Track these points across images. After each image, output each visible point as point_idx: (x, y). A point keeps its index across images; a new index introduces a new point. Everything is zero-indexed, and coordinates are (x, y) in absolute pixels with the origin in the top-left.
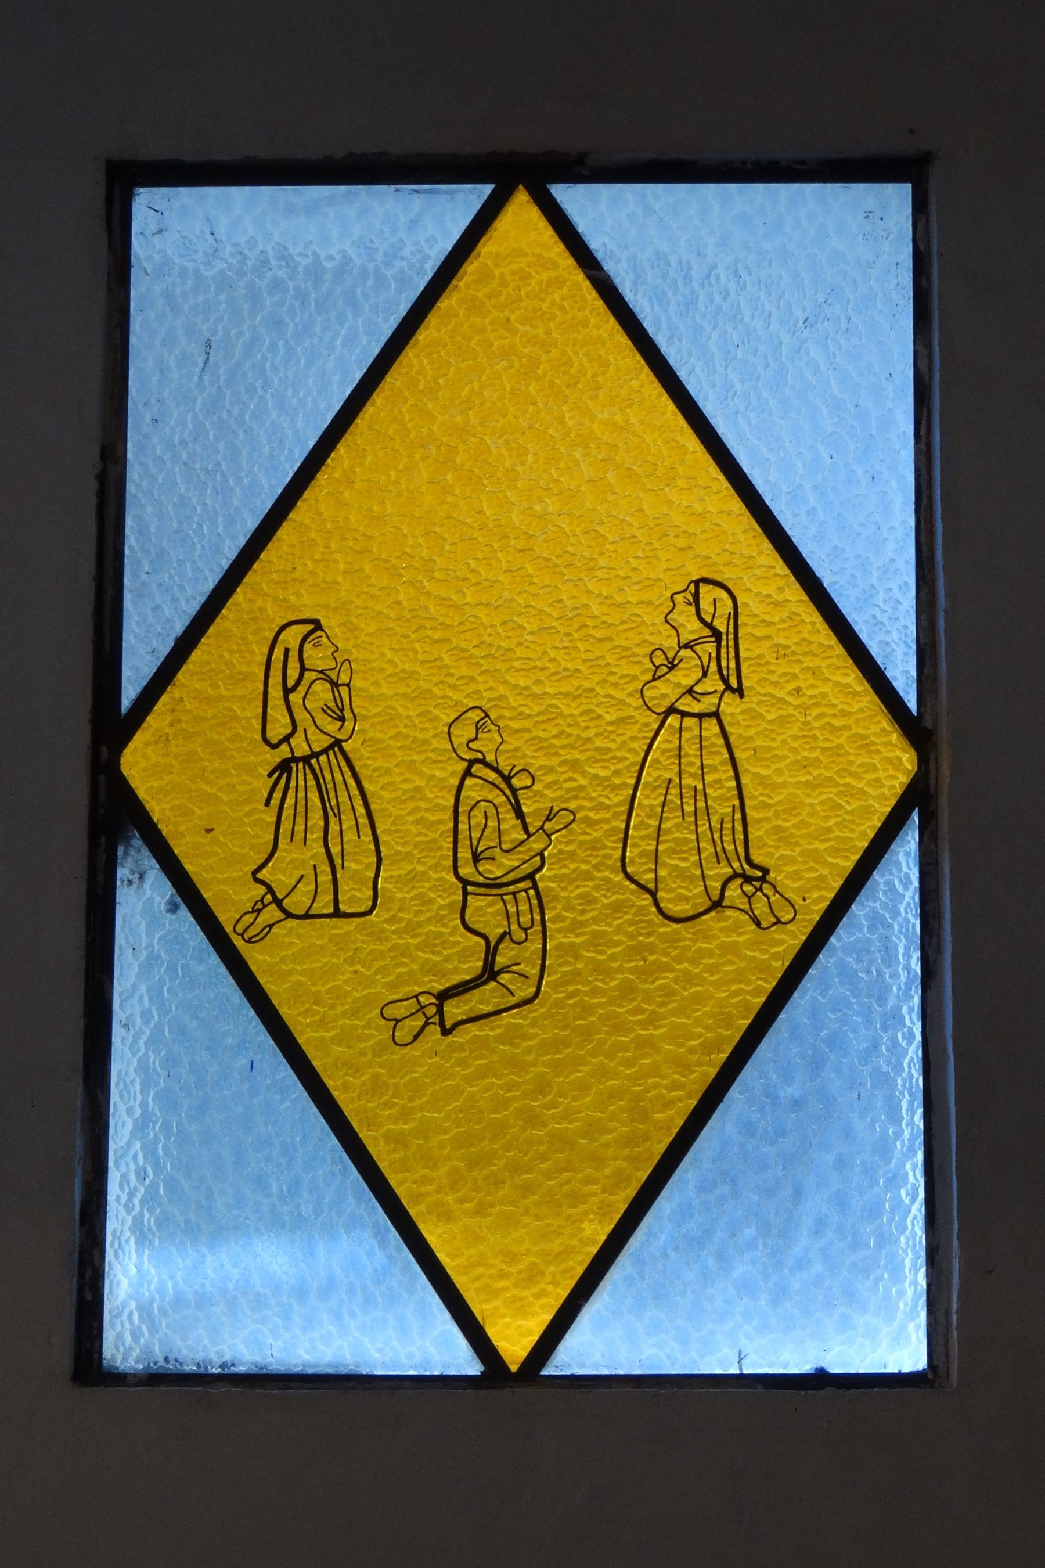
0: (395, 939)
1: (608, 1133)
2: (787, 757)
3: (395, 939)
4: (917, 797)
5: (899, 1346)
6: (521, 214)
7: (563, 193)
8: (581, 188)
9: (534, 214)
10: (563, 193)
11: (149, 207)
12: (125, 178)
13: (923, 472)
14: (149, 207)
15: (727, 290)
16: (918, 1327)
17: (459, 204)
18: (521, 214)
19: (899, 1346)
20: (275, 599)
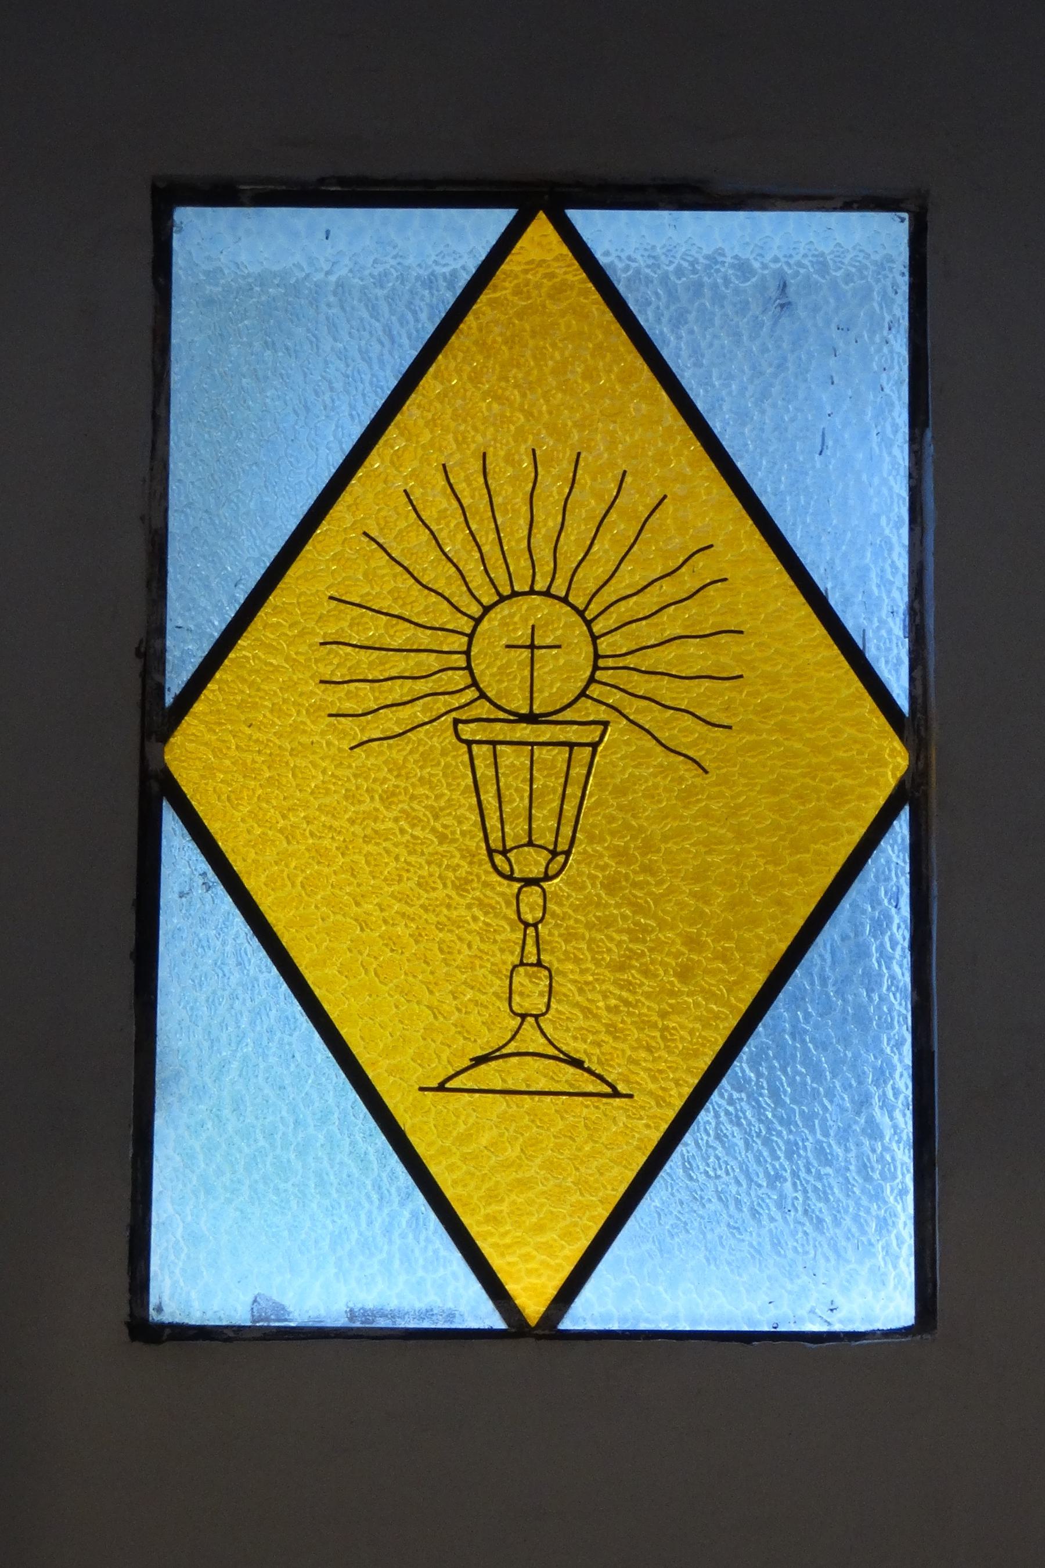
0: (877, 288)
1: (869, 338)
2: (692, 845)
3: (877, 288)
4: (907, 794)
5: (880, 1296)
6: (542, 229)
7: (576, 216)
8: (597, 213)
9: (549, 229)
10: (576, 216)
11: (184, 215)
12: (168, 196)
13: (918, 683)
14: (184, 215)
15: (401, 324)
16: (902, 1193)
17: (492, 222)
18: (542, 229)
19: (880, 1296)
20: (511, 405)
